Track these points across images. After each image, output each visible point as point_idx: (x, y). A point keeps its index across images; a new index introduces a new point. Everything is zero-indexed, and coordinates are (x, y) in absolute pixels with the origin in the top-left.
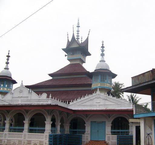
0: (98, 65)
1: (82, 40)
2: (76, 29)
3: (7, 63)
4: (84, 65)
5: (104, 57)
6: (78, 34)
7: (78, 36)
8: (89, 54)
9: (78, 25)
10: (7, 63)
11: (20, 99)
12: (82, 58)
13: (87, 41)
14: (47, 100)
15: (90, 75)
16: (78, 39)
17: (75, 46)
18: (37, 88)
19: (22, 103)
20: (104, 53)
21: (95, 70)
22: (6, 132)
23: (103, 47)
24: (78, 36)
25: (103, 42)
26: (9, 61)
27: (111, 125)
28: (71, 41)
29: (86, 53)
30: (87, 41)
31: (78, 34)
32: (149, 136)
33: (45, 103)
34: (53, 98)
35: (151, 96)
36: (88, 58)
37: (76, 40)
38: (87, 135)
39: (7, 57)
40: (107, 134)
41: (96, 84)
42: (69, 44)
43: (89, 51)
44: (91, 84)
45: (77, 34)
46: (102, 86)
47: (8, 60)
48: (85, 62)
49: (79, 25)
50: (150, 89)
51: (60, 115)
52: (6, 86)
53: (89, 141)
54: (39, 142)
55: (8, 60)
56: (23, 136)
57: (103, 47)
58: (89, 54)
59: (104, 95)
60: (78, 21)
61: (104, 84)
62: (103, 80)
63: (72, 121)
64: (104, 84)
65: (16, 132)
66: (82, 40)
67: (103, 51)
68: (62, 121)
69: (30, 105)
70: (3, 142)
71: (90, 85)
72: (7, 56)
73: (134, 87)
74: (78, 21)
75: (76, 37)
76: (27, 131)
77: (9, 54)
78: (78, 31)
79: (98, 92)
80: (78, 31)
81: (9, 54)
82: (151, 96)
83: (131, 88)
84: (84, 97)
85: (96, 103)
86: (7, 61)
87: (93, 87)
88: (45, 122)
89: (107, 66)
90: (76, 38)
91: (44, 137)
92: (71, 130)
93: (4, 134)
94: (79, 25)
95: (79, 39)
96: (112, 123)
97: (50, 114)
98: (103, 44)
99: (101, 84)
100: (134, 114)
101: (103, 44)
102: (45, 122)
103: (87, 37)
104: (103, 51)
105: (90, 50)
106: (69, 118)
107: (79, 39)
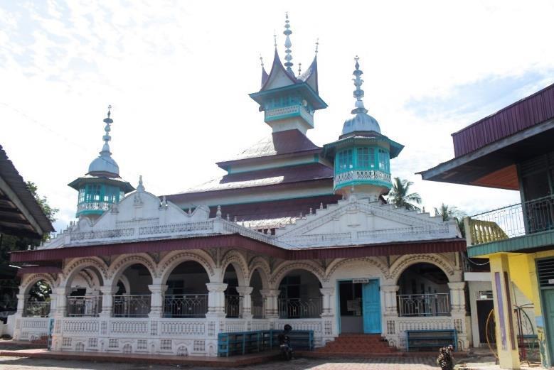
0: (347, 124)
1: (300, 70)
2: (282, 39)
3: (107, 139)
4: (310, 134)
5: (362, 99)
6: (288, 51)
7: (288, 58)
8: (323, 105)
9: (286, 29)
10: (107, 139)
11: (137, 227)
12: (304, 114)
13: (314, 67)
14: (211, 224)
15: (330, 152)
16: (289, 65)
17: (282, 83)
18: (185, 201)
19: (142, 236)
20: (362, 88)
21: (340, 137)
22: (155, 316)
23: (358, 73)
24: (288, 58)
25: (357, 59)
26: (110, 134)
27: (395, 288)
28: (271, 74)
29: (317, 103)
30: (314, 67)
31: (288, 51)
32: (522, 314)
33: (205, 233)
34: (228, 218)
35: (519, 192)
36: (318, 115)
37: (286, 68)
38: (329, 319)
39: (106, 124)
40: (385, 315)
41: (345, 175)
42: (266, 79)
43: (320, 95)
44: (331, 180)
45: (286, 54)
46: (364, 179)
47: (108, 129)
48: (311, 127)
49: (289, 29)
50: (514, 165)
51: (249, 266)
52: (114, 199)
53: (336, 338)
54: (192, 342)
55: (108, 129)
56: (150, 326)
57: (358, 73)
58: (323, 105)
59: (365, 203)
60: (287, 17)
61: (368, 173)
62: (364, 165)
63: (283, 282)
64: (368, 173)
65: (121, 316)
66: (300, 70)
67: (358, 83)
68: (256, 283)
69: (152, 239)
70: (99, 344)
71: (329, 182)
73: (463, 161)
74: (287, 17)
75: (283, 62)
76: (159, 312)
77: (109, 114)
78: (288, 45)
79: (352, 198)
80: (288, 45)
81: (109, 114)
82: (519, 192)
83: (455, 165)
84: (314, 212)
85: (349, 226)
86: (105, 133)
87: (339, 181)
88: (207, 284)
89: (373, 121)
90: (286, 64)
91: (207, 327)
92: (21, 305)
93: (100, 323)
94: (289, 29)
95: (292, 64)
96: (398, 284)
97: (221, 264)
98: (357, 66)
99: (360, 173)
100: (469, 244)
101: (357, 66)
102: (207, 284)
103: (313, 60)
104: (358, 83)
105: (323, 94)
106: (275, 272)
107: (292, 64)
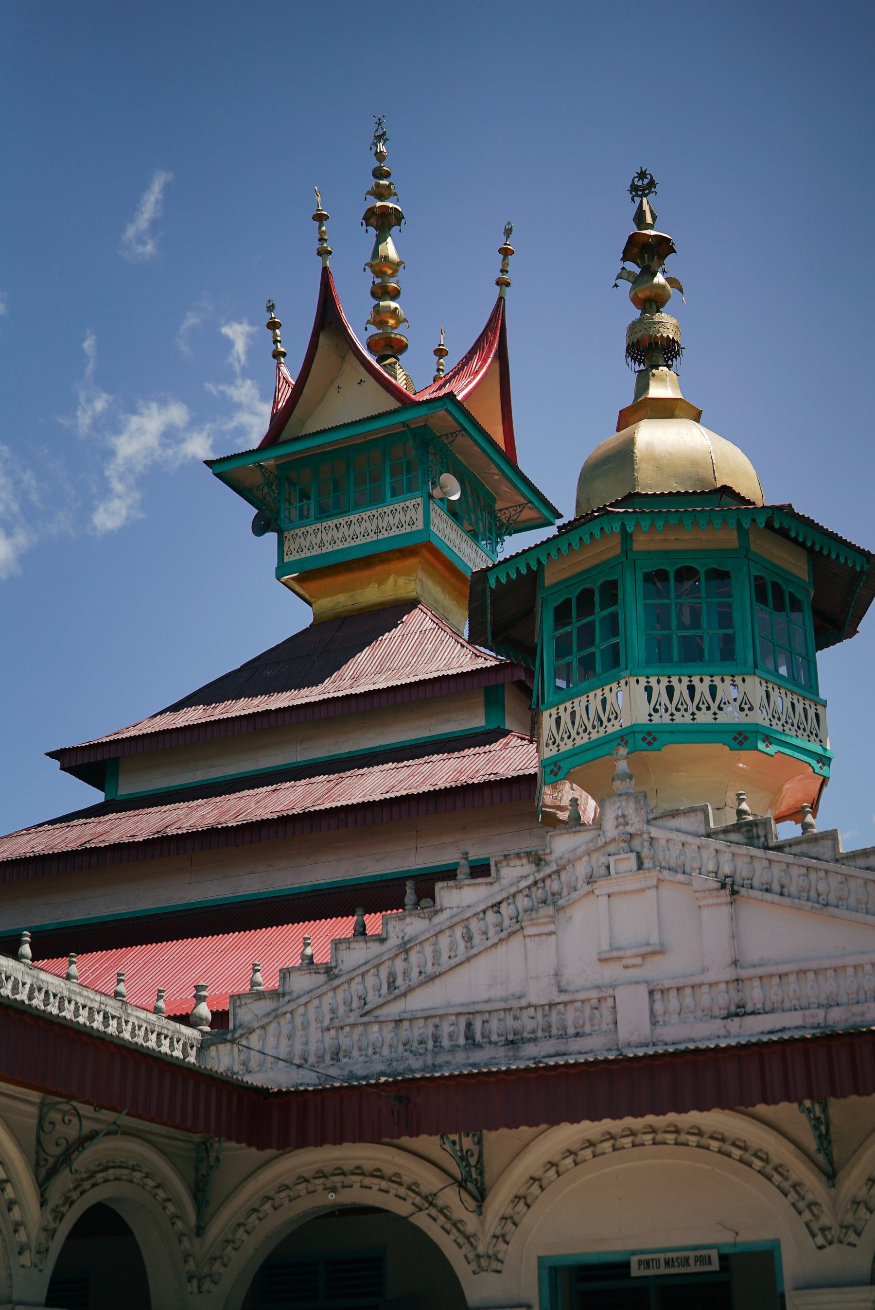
72: (508, 284)
99: (659, 689)
